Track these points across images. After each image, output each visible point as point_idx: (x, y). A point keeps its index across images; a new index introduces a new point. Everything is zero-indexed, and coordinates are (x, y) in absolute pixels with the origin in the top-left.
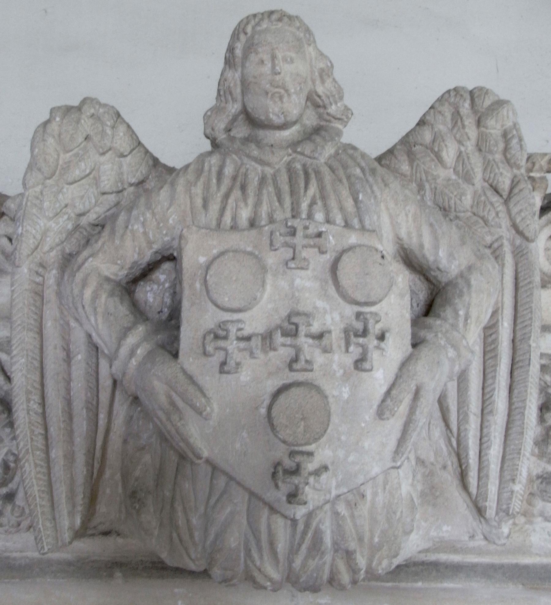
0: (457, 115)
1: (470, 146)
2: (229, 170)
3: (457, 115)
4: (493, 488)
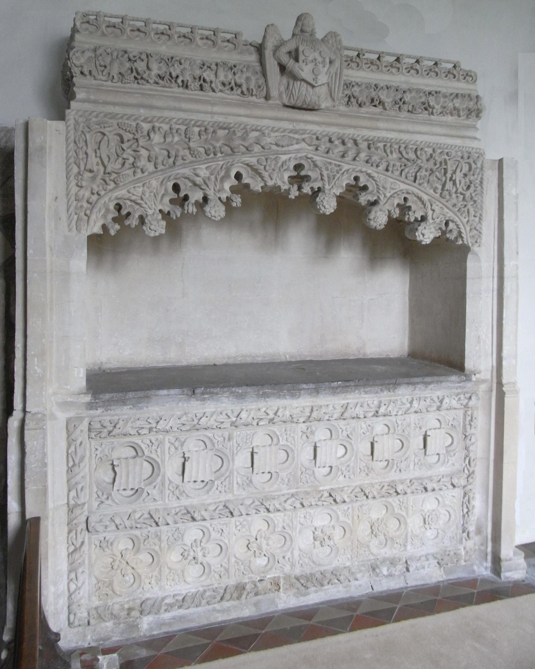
0: (332, 36)
1: (334, 41)
2: (301, 38)
3: (332, 36)
4: (336, 95)
